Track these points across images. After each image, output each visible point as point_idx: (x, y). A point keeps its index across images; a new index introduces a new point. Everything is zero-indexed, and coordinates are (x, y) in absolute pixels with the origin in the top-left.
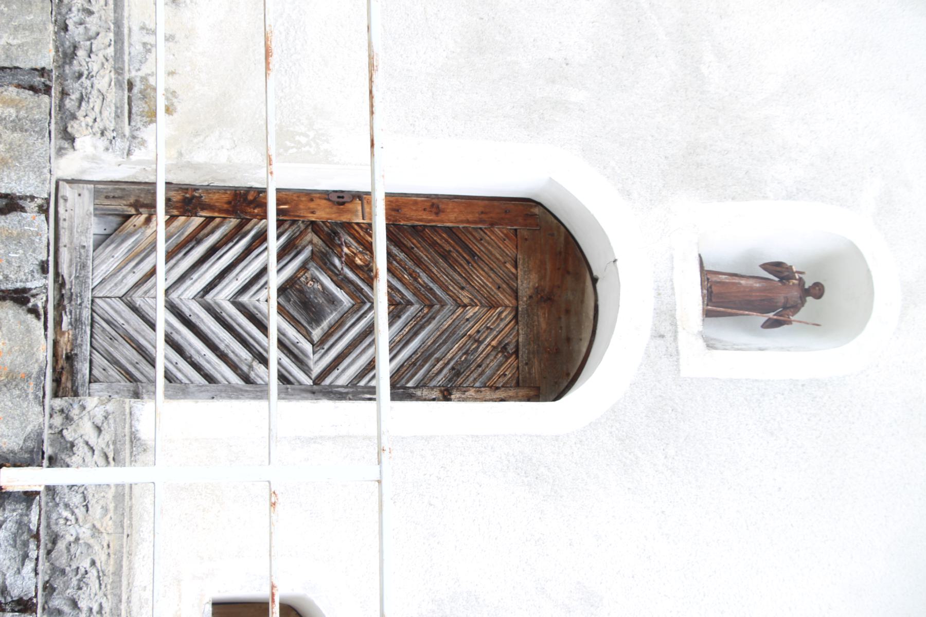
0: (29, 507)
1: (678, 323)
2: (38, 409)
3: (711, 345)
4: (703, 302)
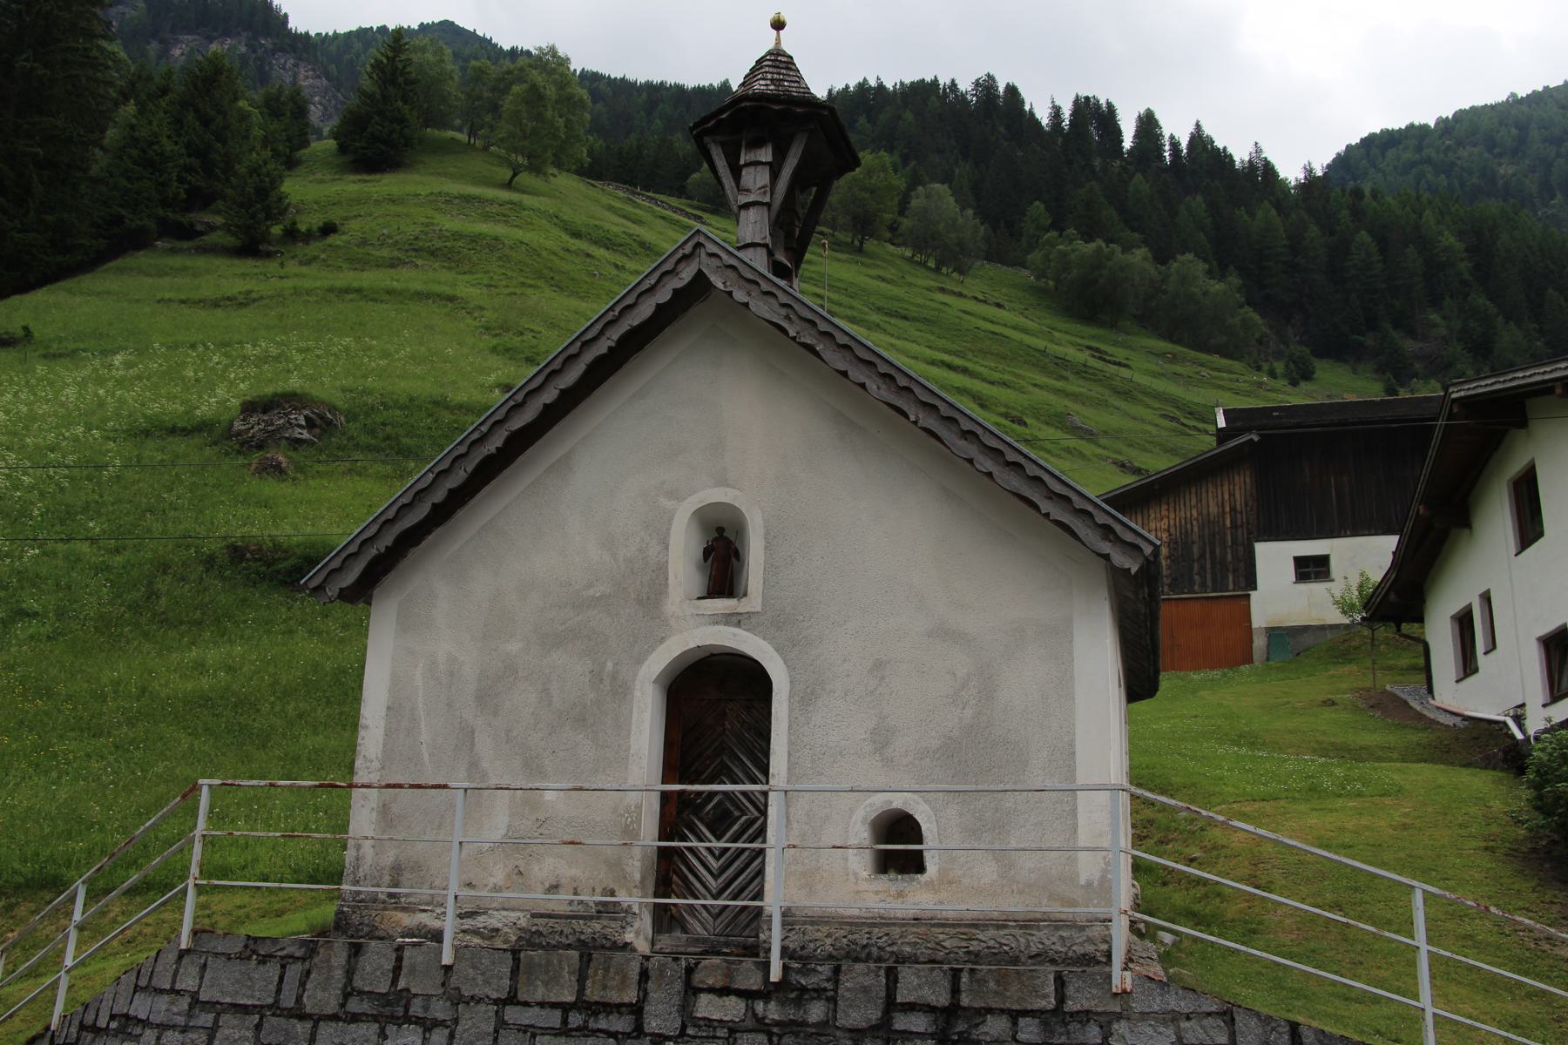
0: (791, 968)
2: (744, 964)
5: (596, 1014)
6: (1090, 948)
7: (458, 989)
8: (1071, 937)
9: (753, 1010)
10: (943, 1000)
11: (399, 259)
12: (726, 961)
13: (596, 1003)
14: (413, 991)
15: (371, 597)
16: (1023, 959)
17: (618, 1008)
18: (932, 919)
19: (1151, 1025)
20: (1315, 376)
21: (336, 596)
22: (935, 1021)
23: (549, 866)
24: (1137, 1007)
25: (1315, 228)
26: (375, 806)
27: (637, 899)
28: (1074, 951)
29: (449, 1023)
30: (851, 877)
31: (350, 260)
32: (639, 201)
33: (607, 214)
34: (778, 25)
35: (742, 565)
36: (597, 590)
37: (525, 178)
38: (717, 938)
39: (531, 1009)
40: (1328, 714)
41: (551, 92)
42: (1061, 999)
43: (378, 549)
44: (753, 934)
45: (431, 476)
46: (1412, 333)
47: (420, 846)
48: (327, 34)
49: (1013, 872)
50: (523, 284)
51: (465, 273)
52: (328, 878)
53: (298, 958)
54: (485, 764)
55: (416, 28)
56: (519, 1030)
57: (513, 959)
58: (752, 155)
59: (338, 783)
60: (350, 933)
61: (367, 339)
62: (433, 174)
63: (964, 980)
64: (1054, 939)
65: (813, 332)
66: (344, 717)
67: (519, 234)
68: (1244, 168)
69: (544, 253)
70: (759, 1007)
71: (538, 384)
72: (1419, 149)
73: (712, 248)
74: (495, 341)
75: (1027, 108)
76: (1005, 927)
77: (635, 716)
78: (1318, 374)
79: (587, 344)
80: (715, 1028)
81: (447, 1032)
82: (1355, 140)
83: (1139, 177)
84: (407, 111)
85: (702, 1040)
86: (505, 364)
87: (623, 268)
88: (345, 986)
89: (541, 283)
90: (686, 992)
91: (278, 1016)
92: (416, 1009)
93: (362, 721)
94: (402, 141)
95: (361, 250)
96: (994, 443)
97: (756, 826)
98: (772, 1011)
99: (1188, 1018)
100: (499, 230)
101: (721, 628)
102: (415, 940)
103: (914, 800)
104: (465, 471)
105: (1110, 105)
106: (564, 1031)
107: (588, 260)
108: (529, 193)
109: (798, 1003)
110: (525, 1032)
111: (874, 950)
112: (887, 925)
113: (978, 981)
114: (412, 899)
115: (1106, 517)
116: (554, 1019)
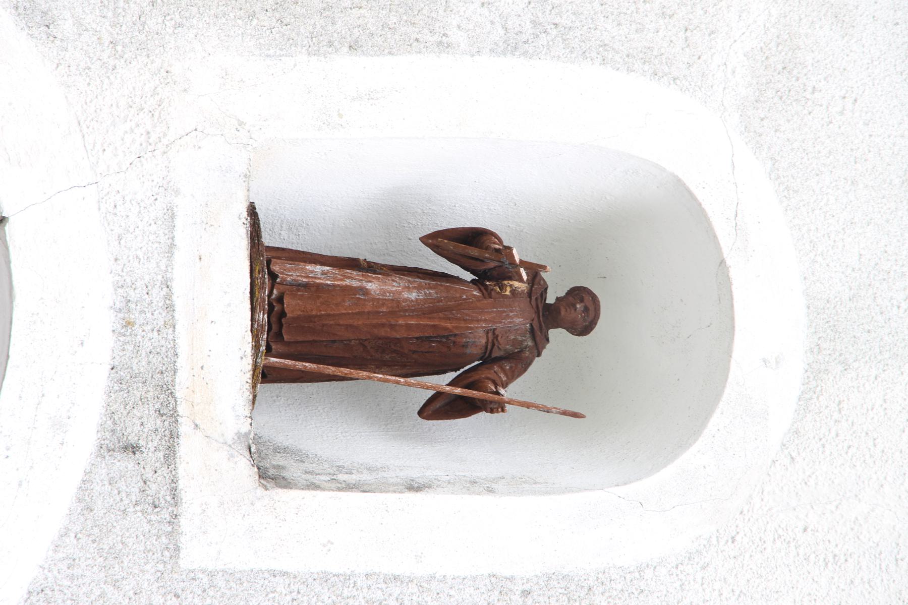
1: (181, 410)
3: (271, 472)
4: (256, 347)
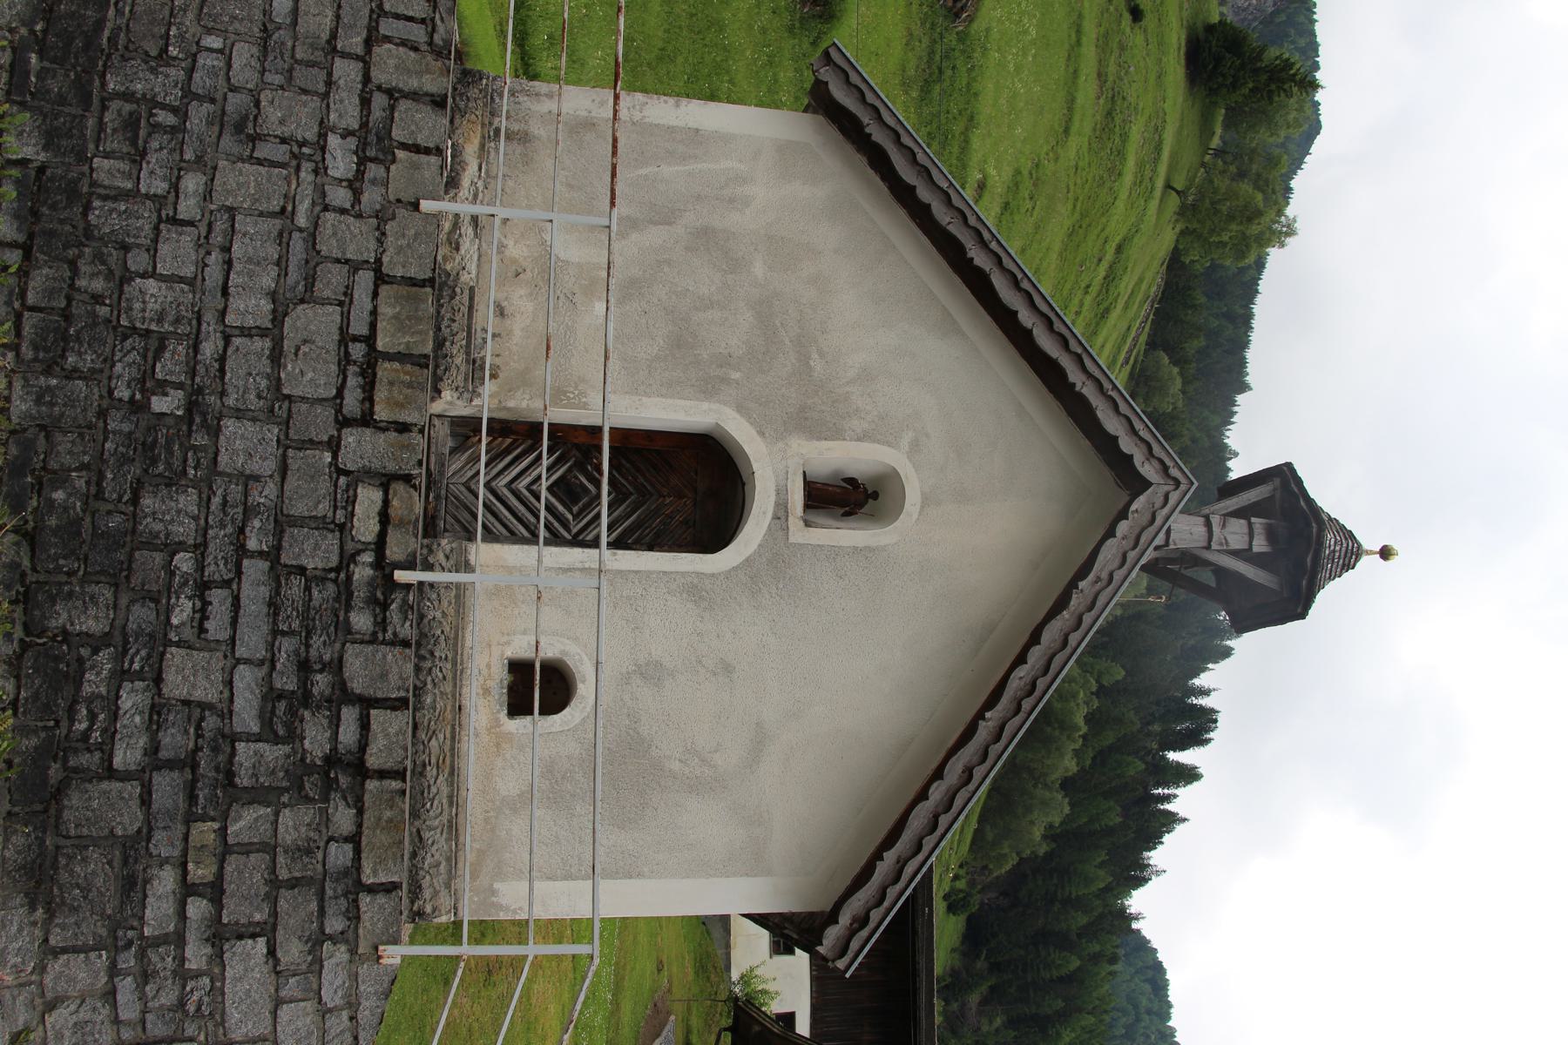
2: (414, 540)
5: (363, 374)
6: (427, 894)
7: (394, 218)
8: (439, 874)
9: (364, 551)
10: (373, 761)
11: (1105, 82)
12: (417, 520)
13: (375, 375)
14: (393, 168)
15: (815, 112)
16: (417, 823)
17: (369, 399)
18: (460, 725)
19: (344, 983)
20: (951, 915)
21: (820, 78)
22: (349, 752)
23: (521, 302)
24: (363, 970)
25: (1085, 921)
26: (593, 114)
27: (487, 402)
28: (424, 877)
29: (357, 208)
30: (505, 639)
31: (1106, 35)
32: (1145, 307)
33: (1136, 278)
34: (1385, 553)
35: (834, 517)
36: (817, 364)
37: (1174, 201)
38: (444, 486)
39: (369, 300)
40: (650, 966)
41: (1254, 229)
42: (372, 890)
43: (868, 125)
44: (447, 526)
45: (945, 185)
46: (984, 1002)
47: (549, 163)
48: (1315, 13)
49: (507, 812)
50: (1076, 199)
51: (1090, 144)
52: (521, 20)
53: (432, 37)
54: (634, 236)
55: (1316, 99)
56: (347, 287)
57: (424, 280)
58: (1261, 531)
59: (619, 83)
60: (459, 86)
61: (1033, 51)
62: (1182, 113)
63: (394, 783)
64: (437, 856)
65: (1082, 608)
66: (677, 30)
67: (1124, 195)
68: (1143, 859)
69: (1104, 220)
70: (368, 557)
71: (1041, 309)
72: (1149, 1012)
73: (1174, 497)
74: (1025, 173)
75: (1210, 666)
76: (451, 804)
77: (682, 402)
78: (953, 918)
79: (1079, 359)
80: (345, 508)
81: (348, 206)
82: (1161, 956)
83: (1141, 766)
84: (1243, 91)
85: (333, 495)
86: (1004, 183)
87: (1086, 293)
88: (400, 91)
89: (1077, 216)
90: (385, 475)
91: (370, 16)
92: (374, 170)
93: (684, 101)
94: (1215, 86)
95: (1115, 45)
96: (958, 802)
97: (562, 530)
98: (362, 572)
99: (351, 1018)
100: (1128, 178)
101: (773, 498)
102: (449, 159)
103: (585, 708)
104: (949, 223)
105: (1208, 741)
106: (345, 338)
107: (1095, 260)
108: (1160, 206)
109: (372, 601)
110: (345, 294)
111: (428, 664)
112: (454, 678)
113: (392, 799)
114: (493, 153)
115: (877, 921)
116: (359, 327)
